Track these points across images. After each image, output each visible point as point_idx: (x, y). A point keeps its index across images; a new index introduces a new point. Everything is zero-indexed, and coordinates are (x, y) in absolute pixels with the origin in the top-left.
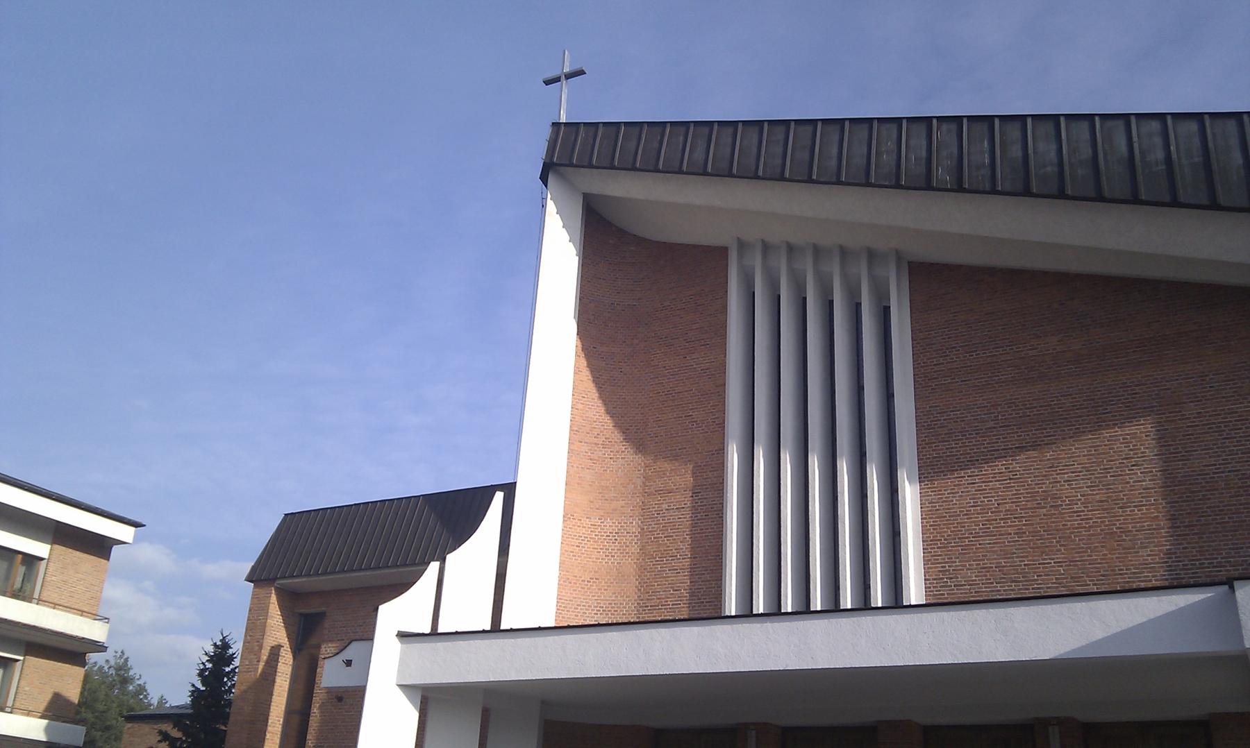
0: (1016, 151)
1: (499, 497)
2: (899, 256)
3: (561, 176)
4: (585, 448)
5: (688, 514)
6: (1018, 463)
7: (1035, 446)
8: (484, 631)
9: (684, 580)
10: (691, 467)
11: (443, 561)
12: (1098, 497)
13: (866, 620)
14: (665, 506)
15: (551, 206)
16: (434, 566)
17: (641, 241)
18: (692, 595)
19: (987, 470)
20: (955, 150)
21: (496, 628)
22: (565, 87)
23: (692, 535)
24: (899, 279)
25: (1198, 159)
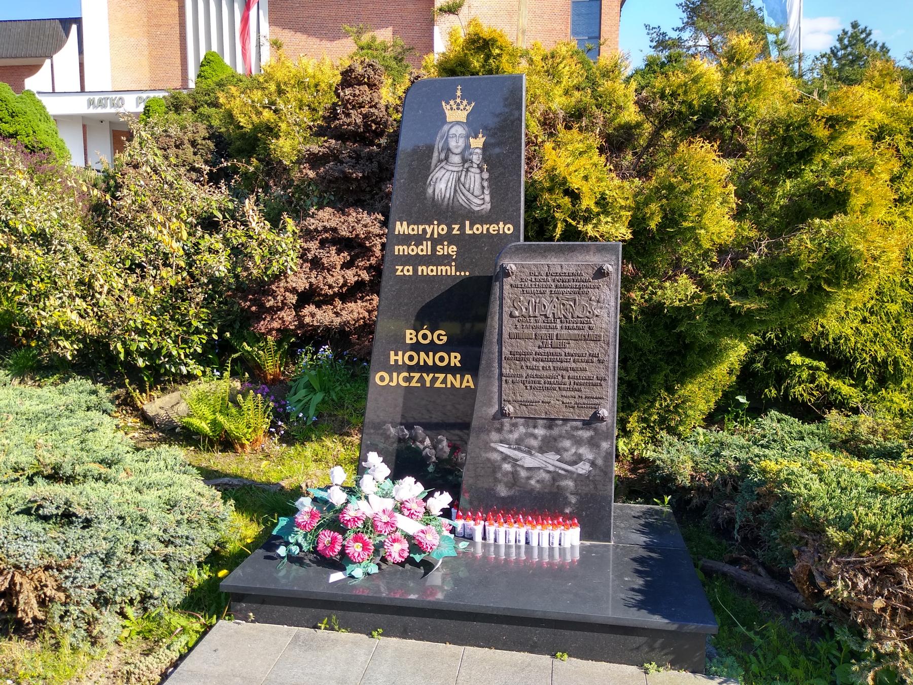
1: (74, 28)
14: (159, 33)
16: (48, 62)
21: (83, 90)
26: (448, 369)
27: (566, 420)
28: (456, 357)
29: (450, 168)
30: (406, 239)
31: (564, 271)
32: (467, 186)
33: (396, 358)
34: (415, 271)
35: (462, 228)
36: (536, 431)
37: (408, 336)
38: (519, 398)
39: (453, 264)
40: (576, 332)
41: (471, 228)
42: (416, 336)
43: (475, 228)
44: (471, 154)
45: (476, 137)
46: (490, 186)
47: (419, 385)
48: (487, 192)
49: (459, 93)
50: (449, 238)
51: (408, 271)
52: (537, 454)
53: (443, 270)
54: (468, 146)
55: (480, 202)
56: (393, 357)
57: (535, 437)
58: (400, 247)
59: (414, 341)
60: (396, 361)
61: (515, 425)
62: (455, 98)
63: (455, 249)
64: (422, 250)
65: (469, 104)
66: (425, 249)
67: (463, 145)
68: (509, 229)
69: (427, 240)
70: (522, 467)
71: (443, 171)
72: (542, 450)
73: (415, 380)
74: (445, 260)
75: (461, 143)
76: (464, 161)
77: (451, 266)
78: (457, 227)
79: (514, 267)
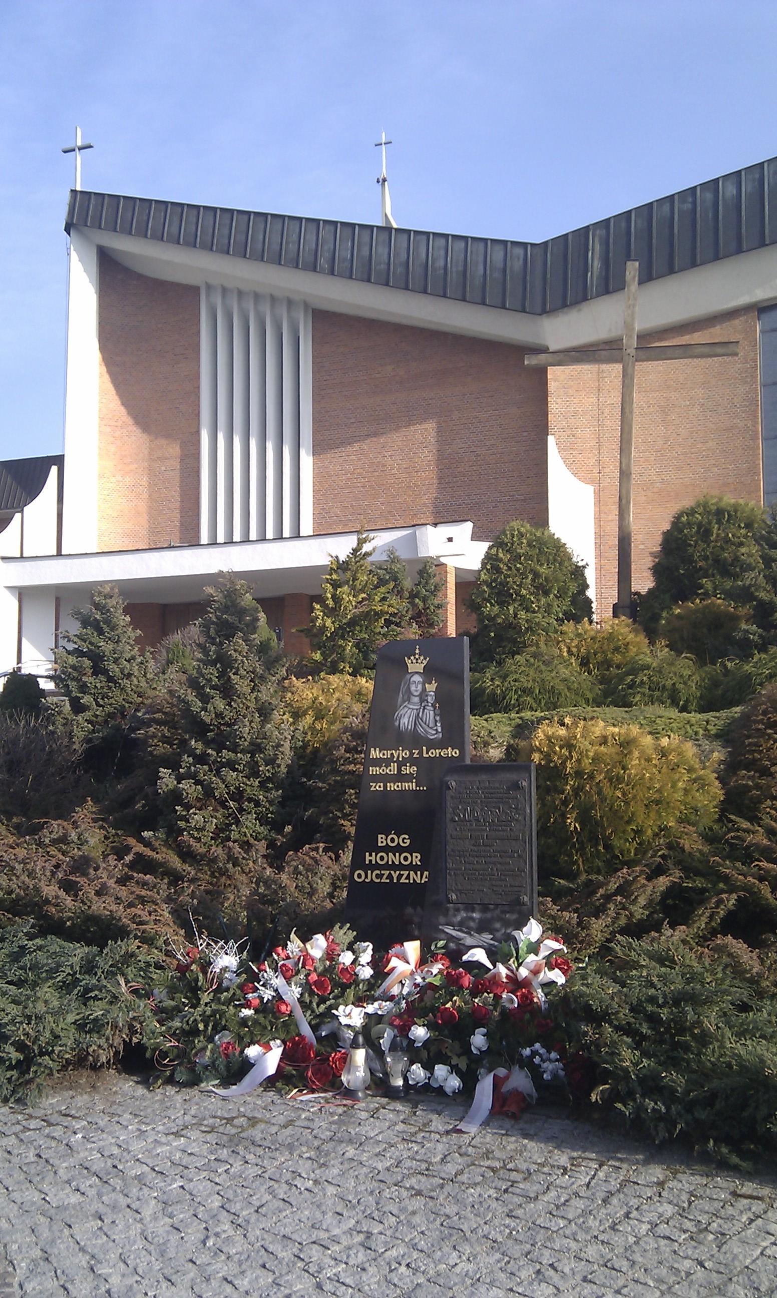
0: (365, 252)
1: (54, 469)
2: (306, 305)
3: (79, 231)
4: (108, 429)
5: (177, 473)
6: (366, 445)
7: (375, 434)
8: (53, 556)
9: (176, 516)
10: (179, 442)
11: (22, 511)
12: (405, 466)
13: (248, 547)
14: (163, 468)
15: (74, 255)
16: (18, 516)
17: (140, 277)
18: (182, 525)
19: (349, 449)
20: (332, 247)
21: (59, 554)
22: (79, 156)
23: (180, 487)
24: (305, 323)
25: (461, 268)
26: (411, 867)
27: (497, 905)
28: (417, 857)
29: (411, 707)
30: (377, 762)
31: (491, 785)
32: (424, 720)
33: (370, 858)
34: (385, 787)
35: (421, 753)
36: (474, 915)
37: (380, 840)
38: (460, 887)
39: (414, 781)
40: (501, 833)
41: (427, 753)
42: (386, 840)
43: (430, 754)
44: (427, 696)
45: (430, 683)
46: (441, 720)
47: (388, 881)
48: (439, 724)
49: (417, 651)
50: (413, 761)
51: (380, 787)
52: (475, 934)
53: (406, 785)
54: (424, 689)
55: (434, 732)
56: (368, 858)
57: (473, 919)
58: (374, 768)
59: (384, 844)
60: (371, 861)
61: (458, 910)
62: (414, 655)
63: (415, 769)
64: (390, 771)
65: (425, 659)
66: (393, 769)
67: (421, 690)
68: (456, 753)
69: (394, 762)
70: (464, 945)
71: (406, 709)
72: (480, 930)
73: (385, 877)
74: (408, 778)
75: (420, 687)
76: (421, 701)
77: (412, 782)
78: (417, 752)
79: (454, 784)
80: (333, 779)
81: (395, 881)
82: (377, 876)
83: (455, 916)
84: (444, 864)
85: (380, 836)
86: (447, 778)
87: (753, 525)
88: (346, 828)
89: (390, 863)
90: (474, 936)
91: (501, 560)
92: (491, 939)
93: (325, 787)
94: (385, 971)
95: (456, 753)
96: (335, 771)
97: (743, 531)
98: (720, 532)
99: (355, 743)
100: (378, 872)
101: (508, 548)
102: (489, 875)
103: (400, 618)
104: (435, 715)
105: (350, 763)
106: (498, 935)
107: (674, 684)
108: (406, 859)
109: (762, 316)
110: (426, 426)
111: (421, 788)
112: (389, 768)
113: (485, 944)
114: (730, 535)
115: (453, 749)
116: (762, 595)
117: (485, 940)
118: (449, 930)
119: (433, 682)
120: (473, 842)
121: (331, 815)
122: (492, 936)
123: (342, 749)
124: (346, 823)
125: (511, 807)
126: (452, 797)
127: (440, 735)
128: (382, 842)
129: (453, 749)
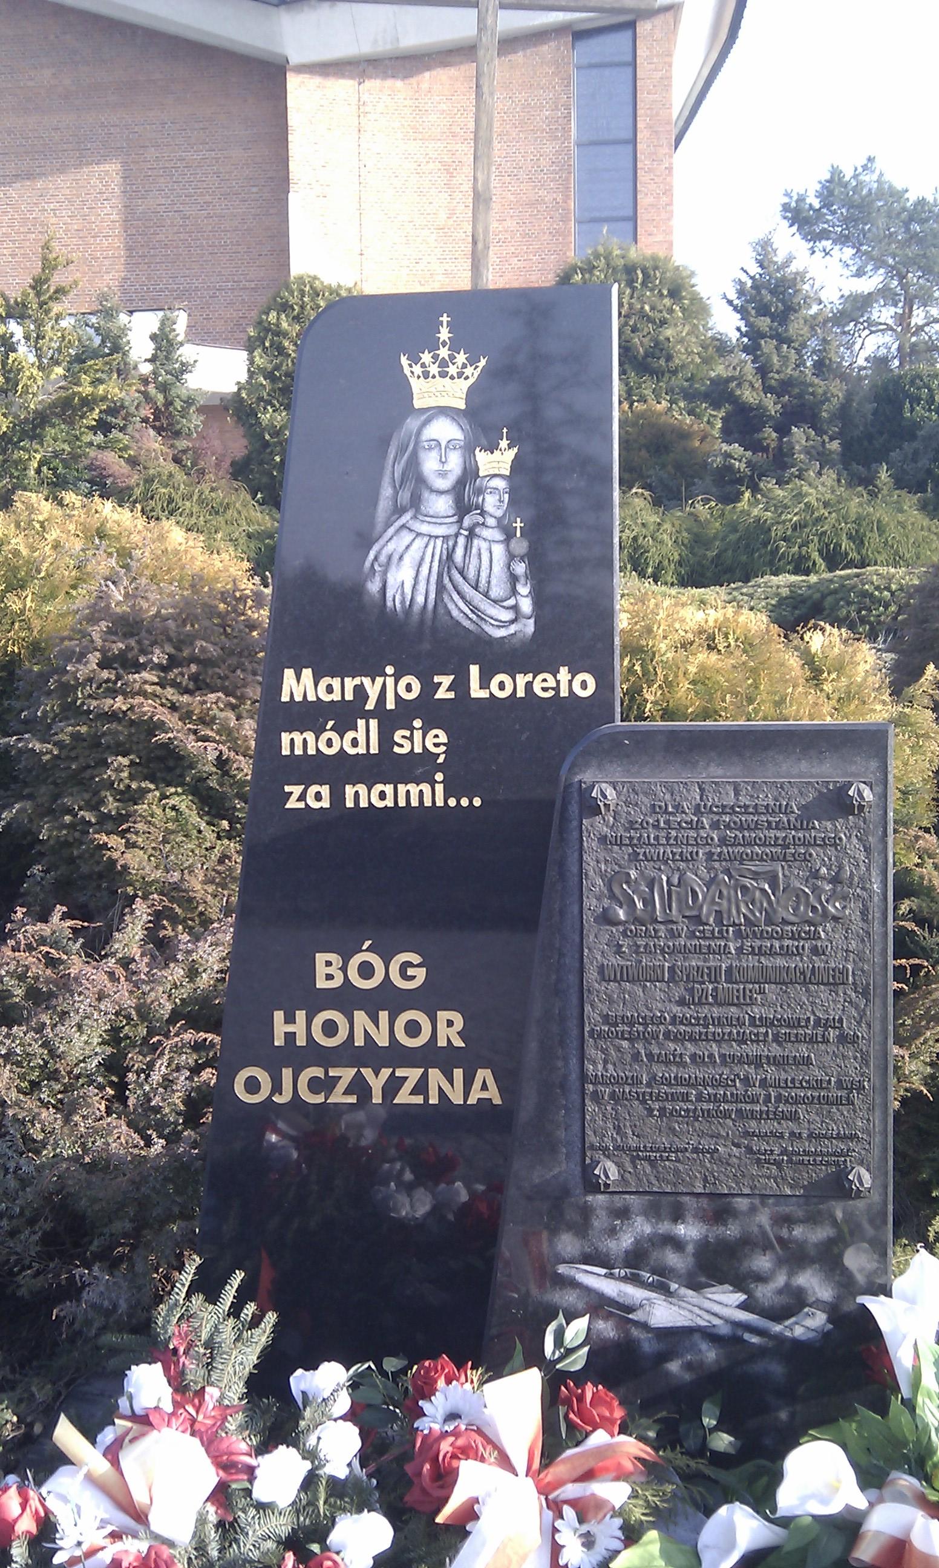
7: (30, 176)
12: (76, 227)
28: (450, 1023)
29: (424, 528)
31: (744, 800)
32: (471, 573)
34: (338, 796)
35: (461, 685)
36: (681, 1230)
37: (321, 970)
39: (439, 777)
40: (780, 962)
42: (344, 969)
44: (480, 491)
45: (492, 448)
48: (524, 589)
49: (444, 334)
51: (318, 797)
52: (684, 1291)
54: (470, 474)
55: (507, 616)
56: (280, 1028)
57: (677, 1244)
61: (624, 1214)
63: (443, 738)
64: (355, 743)
65: (472, 361)
69: (367, 715)
70: (644, 1326)
71: (406, 537)
75: (455, 462)
76: (462, 508)
77: (433, 783)
79: (610, 793)
80: (66, 732)
81: (377, 1099)
82: (315, 1085)
83: (612, 1232)
84: (574, 1062)
85: (321, 958)
86: (587, 776)
87: (680, 292)
88: (116, 855)
89: (359, 1042)
90: (681, 1298)
91: (285, 334)
92: (743, 1306)
93: (50, 752)
94: (439, 1519)
95: (585, 685)
96: (72, 711)
97: (667, 302)
98: (633, 301)
99: (121, 645)
100: (317, 1072)
101: (296, 313)
102: (736, 1099)
103: (124, 419)
104: (511, 557)
105: (113, 693)
106: (765, 1293)
107: (635, 539)
108: (413, 1029)
109: (577, 44)
110: (107, 167)
111: (464, 802)
112: (350, 735)
113: (716, 1321)
114: (647, 308)
115: (574, 673)
116: (749, 396)
117: (717, 1308)
118: (594, 1279)
119: (504, 443)
120: (678, 992)
121: (68, 818)
122: (741, 1297)
123: (94, 658)
124: (114, 841)
125: (816, 875)
126: (603, 839)
127: (530, 627)
128: (329, 977)
129: (574, 673)
